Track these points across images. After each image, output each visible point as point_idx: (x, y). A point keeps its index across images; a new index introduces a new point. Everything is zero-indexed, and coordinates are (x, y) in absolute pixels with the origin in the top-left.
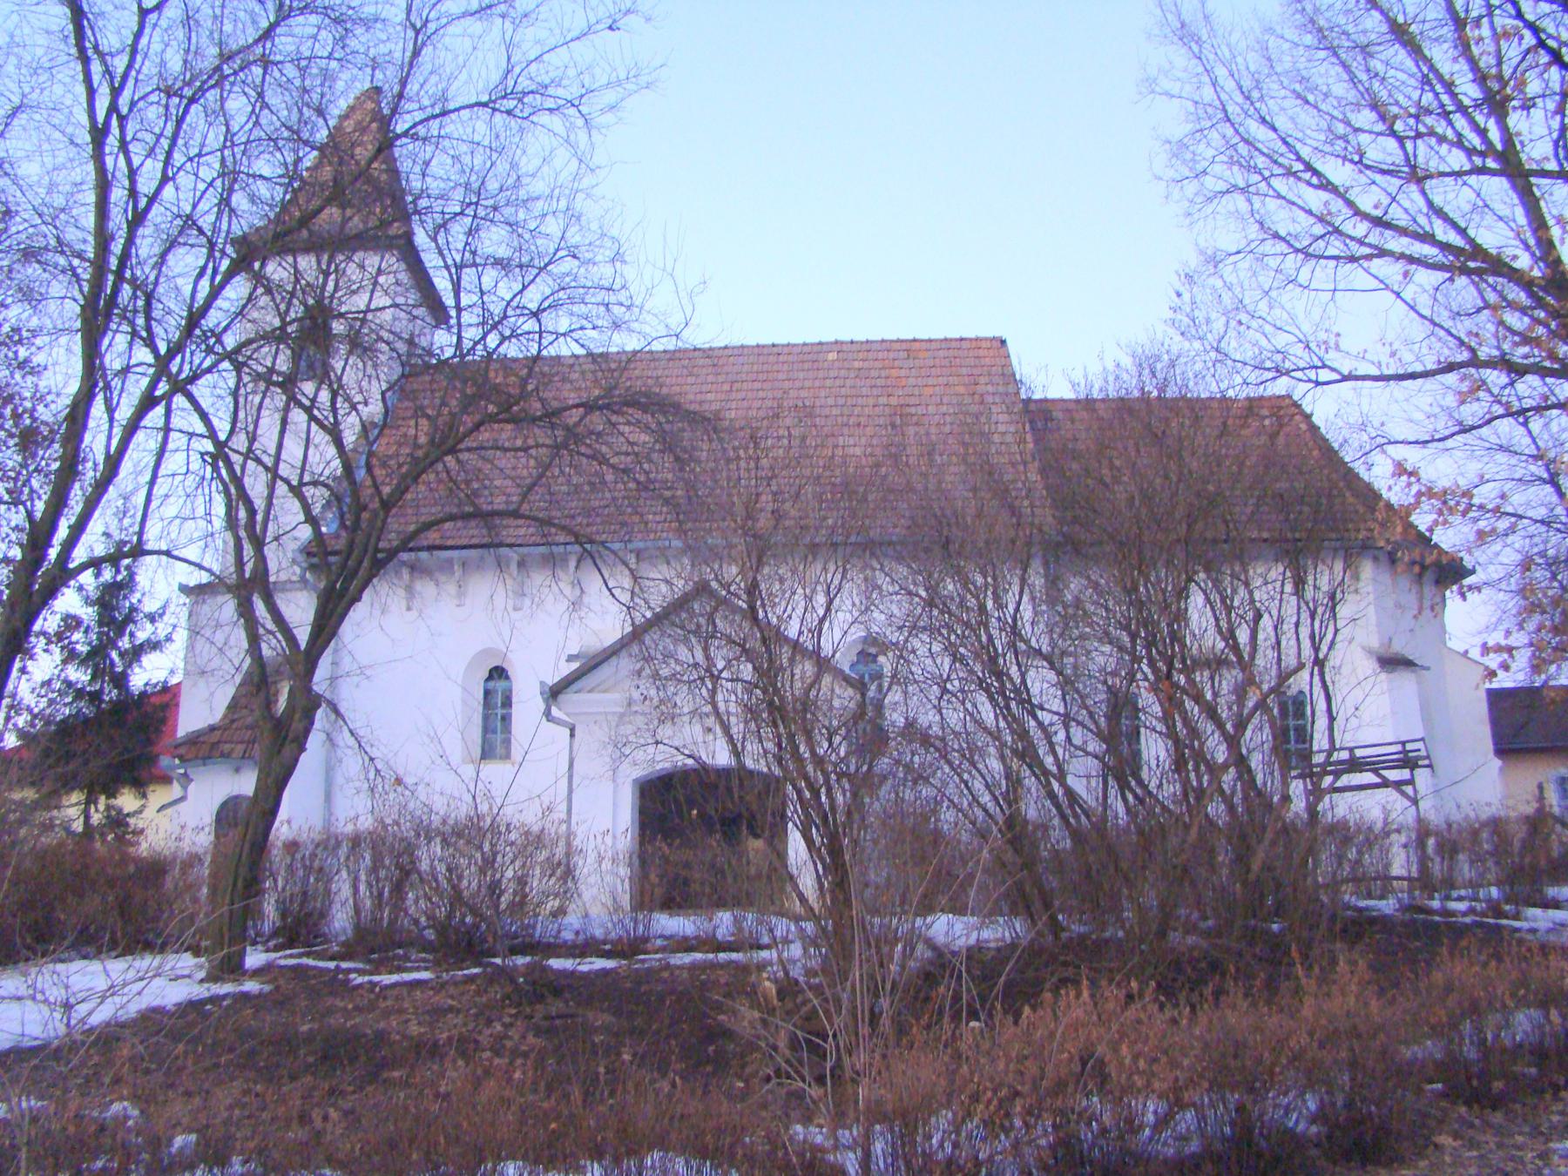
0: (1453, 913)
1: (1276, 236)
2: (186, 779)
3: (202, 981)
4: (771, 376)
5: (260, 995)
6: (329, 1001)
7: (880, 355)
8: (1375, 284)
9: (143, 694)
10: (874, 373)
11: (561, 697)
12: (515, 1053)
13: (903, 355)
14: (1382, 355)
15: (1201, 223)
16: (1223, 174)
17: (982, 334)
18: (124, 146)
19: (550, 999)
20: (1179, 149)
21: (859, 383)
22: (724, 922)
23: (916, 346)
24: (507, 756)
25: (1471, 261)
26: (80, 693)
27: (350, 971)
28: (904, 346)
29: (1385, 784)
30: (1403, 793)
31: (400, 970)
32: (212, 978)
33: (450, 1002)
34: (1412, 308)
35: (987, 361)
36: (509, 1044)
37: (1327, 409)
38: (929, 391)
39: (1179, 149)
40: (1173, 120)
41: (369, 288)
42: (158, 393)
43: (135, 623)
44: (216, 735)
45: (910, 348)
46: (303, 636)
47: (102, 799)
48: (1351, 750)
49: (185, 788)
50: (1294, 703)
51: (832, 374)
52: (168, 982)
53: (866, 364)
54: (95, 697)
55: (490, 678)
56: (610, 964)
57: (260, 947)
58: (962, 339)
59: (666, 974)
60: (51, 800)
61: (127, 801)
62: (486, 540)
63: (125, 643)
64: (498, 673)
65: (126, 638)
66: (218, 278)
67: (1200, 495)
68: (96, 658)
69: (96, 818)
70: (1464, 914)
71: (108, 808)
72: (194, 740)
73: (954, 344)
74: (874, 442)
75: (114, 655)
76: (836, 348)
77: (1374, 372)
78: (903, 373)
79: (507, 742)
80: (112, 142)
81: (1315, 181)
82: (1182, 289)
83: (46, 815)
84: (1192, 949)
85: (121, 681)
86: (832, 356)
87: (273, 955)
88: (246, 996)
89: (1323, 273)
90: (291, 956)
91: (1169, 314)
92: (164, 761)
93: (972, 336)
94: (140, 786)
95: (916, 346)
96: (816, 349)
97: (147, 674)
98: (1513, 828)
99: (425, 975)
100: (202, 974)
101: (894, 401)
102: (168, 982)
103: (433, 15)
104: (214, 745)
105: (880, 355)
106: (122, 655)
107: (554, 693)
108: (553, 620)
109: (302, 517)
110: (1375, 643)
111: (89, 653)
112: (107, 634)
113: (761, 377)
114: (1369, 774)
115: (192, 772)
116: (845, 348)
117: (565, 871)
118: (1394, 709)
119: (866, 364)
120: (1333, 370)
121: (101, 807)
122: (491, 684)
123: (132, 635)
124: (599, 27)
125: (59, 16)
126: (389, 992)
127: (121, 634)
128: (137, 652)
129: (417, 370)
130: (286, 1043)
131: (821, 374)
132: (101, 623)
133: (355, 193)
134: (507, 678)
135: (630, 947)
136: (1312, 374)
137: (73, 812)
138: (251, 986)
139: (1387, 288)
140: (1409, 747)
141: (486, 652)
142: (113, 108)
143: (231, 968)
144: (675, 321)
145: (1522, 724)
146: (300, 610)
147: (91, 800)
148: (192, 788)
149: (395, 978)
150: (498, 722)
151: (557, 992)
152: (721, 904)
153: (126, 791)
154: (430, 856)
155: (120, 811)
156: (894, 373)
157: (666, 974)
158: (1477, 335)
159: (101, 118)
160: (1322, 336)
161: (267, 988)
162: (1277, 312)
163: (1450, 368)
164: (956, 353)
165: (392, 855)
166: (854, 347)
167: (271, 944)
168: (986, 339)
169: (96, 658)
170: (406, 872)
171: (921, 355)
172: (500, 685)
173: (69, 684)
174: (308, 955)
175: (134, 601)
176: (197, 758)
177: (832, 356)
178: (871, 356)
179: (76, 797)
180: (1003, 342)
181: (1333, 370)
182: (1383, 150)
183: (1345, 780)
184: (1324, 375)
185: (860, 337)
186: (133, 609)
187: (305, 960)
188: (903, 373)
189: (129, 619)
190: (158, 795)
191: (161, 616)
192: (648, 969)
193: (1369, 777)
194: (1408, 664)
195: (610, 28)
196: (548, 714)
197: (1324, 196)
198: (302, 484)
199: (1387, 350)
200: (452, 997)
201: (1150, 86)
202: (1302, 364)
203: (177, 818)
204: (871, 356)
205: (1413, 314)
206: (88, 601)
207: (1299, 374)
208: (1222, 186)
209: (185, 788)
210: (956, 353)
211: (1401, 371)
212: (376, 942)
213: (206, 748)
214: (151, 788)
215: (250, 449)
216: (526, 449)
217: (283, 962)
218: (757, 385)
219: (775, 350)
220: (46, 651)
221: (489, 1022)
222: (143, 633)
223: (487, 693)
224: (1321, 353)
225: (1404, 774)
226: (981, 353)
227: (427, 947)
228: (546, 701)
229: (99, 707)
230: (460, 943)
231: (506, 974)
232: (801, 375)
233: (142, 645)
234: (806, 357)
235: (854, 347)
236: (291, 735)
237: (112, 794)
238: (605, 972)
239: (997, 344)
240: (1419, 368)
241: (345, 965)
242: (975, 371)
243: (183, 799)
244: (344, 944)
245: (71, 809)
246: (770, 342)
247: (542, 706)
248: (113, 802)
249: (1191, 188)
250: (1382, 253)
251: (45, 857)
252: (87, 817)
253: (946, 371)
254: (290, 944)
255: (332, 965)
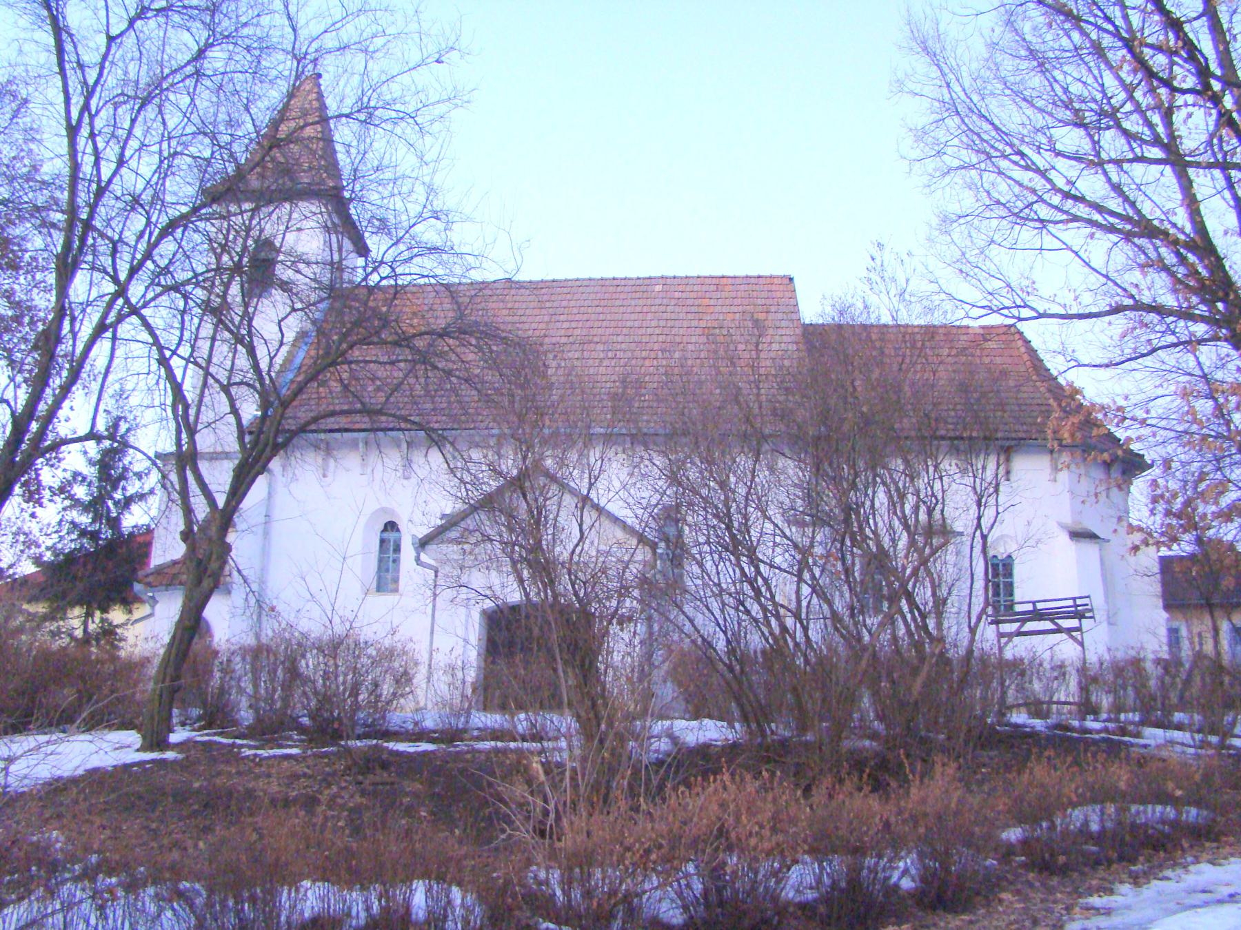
0: (1090, 731)
1: (998, 202)
2: (154, 601)
3: (138, 750)
4: (610, 303)
5: (175, 761)
6: (222, 766)
7: (696, 288)
8: (1059, 245)
9: (131, 534)
10: (689, 302)
11: (429, 547)
12: (343, 807)
13: (713, 288)
14: (1068, 298)
15: (939, 192)
16: (959, 154)
17: (775, 273)
18: (93, 136)
19: (378, 771)
20: (920, 135)
21: (677, 309)
22: (522, 721)
23: (724, 281)
24: (396, 590)
25: (1142, 229)
26: (84, 533)
27: (242, 746)
28: (714, 281)
29: (1059, 630)
30: (1072, 637)
31: (280, 746)
32: (142, 749)
33: (306, 770)
34: (1087, 264)
35: (778, 294)
36: (339, 801)
37: (1042, 337)
38: (730, 316)
39: (920, 135)
40: (919, 112)
41: (303, 235)
42: (108, 321)
43: (126, 479)
44: (175, 570)
45: (718, 282)
46: (221, 501)
47: (98, 614)
48: (1034, 603)
49: (153, 607)
50: (1004, 565)
51: (658, 301)
52: (114, 748)
53: (684, 295)
54: (94, 536)
55: (385, 530)
56: (430, 747)
57: (188, 728)
58: (759, 277)
59: (469, 756)
60: (57, 613)
61: (117, 615)
62: (368, 426)
63: (118, 495)
64: (391, 526)
65: (120, 491)
66: (153, 239)
67: (896, 405)
68: (95, 506)
69: (92, 627)
70: (1099, 732)
71: (103, 620)
72: (160, 571)
73: (753, 281)
74: (702, 356)
75: (110, 503)
76: (661, 281)
77: (1063, 312)
78: (712, 302)
79: (396, 580)
80: (85, 132)
81: (1022, 163)
82: (875, 255)
83: (54, 626)
84: (579, 740)
85: (115, 523)
86: (658, 288)
87: (194, 733)
88: (164, 761)
89: (1027, 235)
90: (207, 735)
91: (865, 273)
92: (137, 587)
93: (768, 274)
94: (128, 601)
95: (724, 281)
96: (647, 282)
97: (134, 519)
98: (1149, 666)
99: (295, 751)
100: (138, 746)
101: (703, 324)
102: (114, 748)
103: (310, 50)
104: (174, 576)
105: (696, 288)
106: (116, 503)
107: (423, 544)
108: (418, 488)
109: (228, 410)
110: (1068, 520)
111: (90, 502)
112: (105, 488)
113: (602, 303)
114: (1048, 623)
115: (156, 595)
116: (669, 281)
117: (404, 679)
118: (1056, 571)
119: (684, 295)
120: (1032, 309)
121: (97, 620)
122: (386, 535)
123: (124, 489)
124: (429, 61)
125: (103, 3)
126: (264, 762)
127: (115, 488)
128: (128, 502)
129: (338, 293)
130: (182, 796)
131: (649, 302)
132: (100, 480)
133: (293, 162)
134: (398, 530)
135: (450, 735)
136: (1015, 312)
137: (76, 623)
138: (170, 755)
139: (1069, 248)
140: (1079, 602)
141: (384, 510)
142: (86, 107)
143: (156, 741)
144: (511, 266)
145: (1196, 584)
146: (220, 477)
147: (89, 614)
148: (158, 607)
149: (272, 752)
150: (360, 566)
151: (385, 766)
152: (521, 707)
153: (116, 607)
154: (310, 664)
155: (110, 624)
156: (706, 302)
157: (469, 756)
158: (1137, 286)
159: (75, 114)
160: (1025, 283)
161: (180, 756)
162: (988, 263)
163: (1117, 310)
164: (754, 287)
165: (278, 659)
166: (676, 282)
167: (196, 725)
168: (778, 277)
169: (95, 506)
170: (294, 673)
171: (727, 288)
172: (391, 536)
173: (74, 524)
174: (220, 734)
175: (126, 462)
176: (161, 584)
177: (658, 288)
178: (688, 288)
179: (78, 611)
180: (791, 279)
181: (1032, 309)
182: (1071, 139)
183: (1030, 626)
184: (1025, 313)
185: (681, 273)
186: (125, 469)
187: (217, 738)
188: (712, 302)
189: (122, 477)
190: (140, 611)
191: (146, 475)
192: (458, 753)
193: (1047, 625)
194: (1092, 536)
195: (437, 61)
196: (418, 560)
197: (1031, 174)
198: (230, 385)
199: (1072, 296)
200: (308, 767)
201: (899, 86)
202: (1008, 303)
203: (147, 629)
204: (688, 288)
205: (1087, 270)
206: (91, 463)
207: (1005, 312)
208: (956, 163)
209: (153, 607)
210: (754, 287)
211: (1081, 312)
212: (269, 728)
213: (167, 577)
214: (136, 605)
215: (191, 355)
216: (392, 363)
217: (199, 739)
218: (599, 310)
219: (615, 282)
220: (51, 501)
221: (329, 785)
222: (133, 487)
223: (382, 541)
224: (1024, 296)
225: (1073, 623)
226: (774, 287)
227: (302, 729)
228: (416, 549)
229: (97, 544)
230: (326, 729)
231: (348, 750)
232: (633, 303)
233: (131, 496)
234: (638, 289)
235: (676, 282)
236: (209, 572)
237: (105, 610)
238: (425, 753)
239: (787, 281)
240: (1094, 310)
241: (239, 741)
242: (769, 302)
243: (151, 615)
244: (248, 727)
245: (75, 620)
246: (611, 276)
247: (413, 554)
248: (105, 616)
249: (931, 165)
250: (1075, 219)
251: (46, 655)
252: (85, 624)
253: (746, 302)
254: (209, 725)
255: (230, 741)
